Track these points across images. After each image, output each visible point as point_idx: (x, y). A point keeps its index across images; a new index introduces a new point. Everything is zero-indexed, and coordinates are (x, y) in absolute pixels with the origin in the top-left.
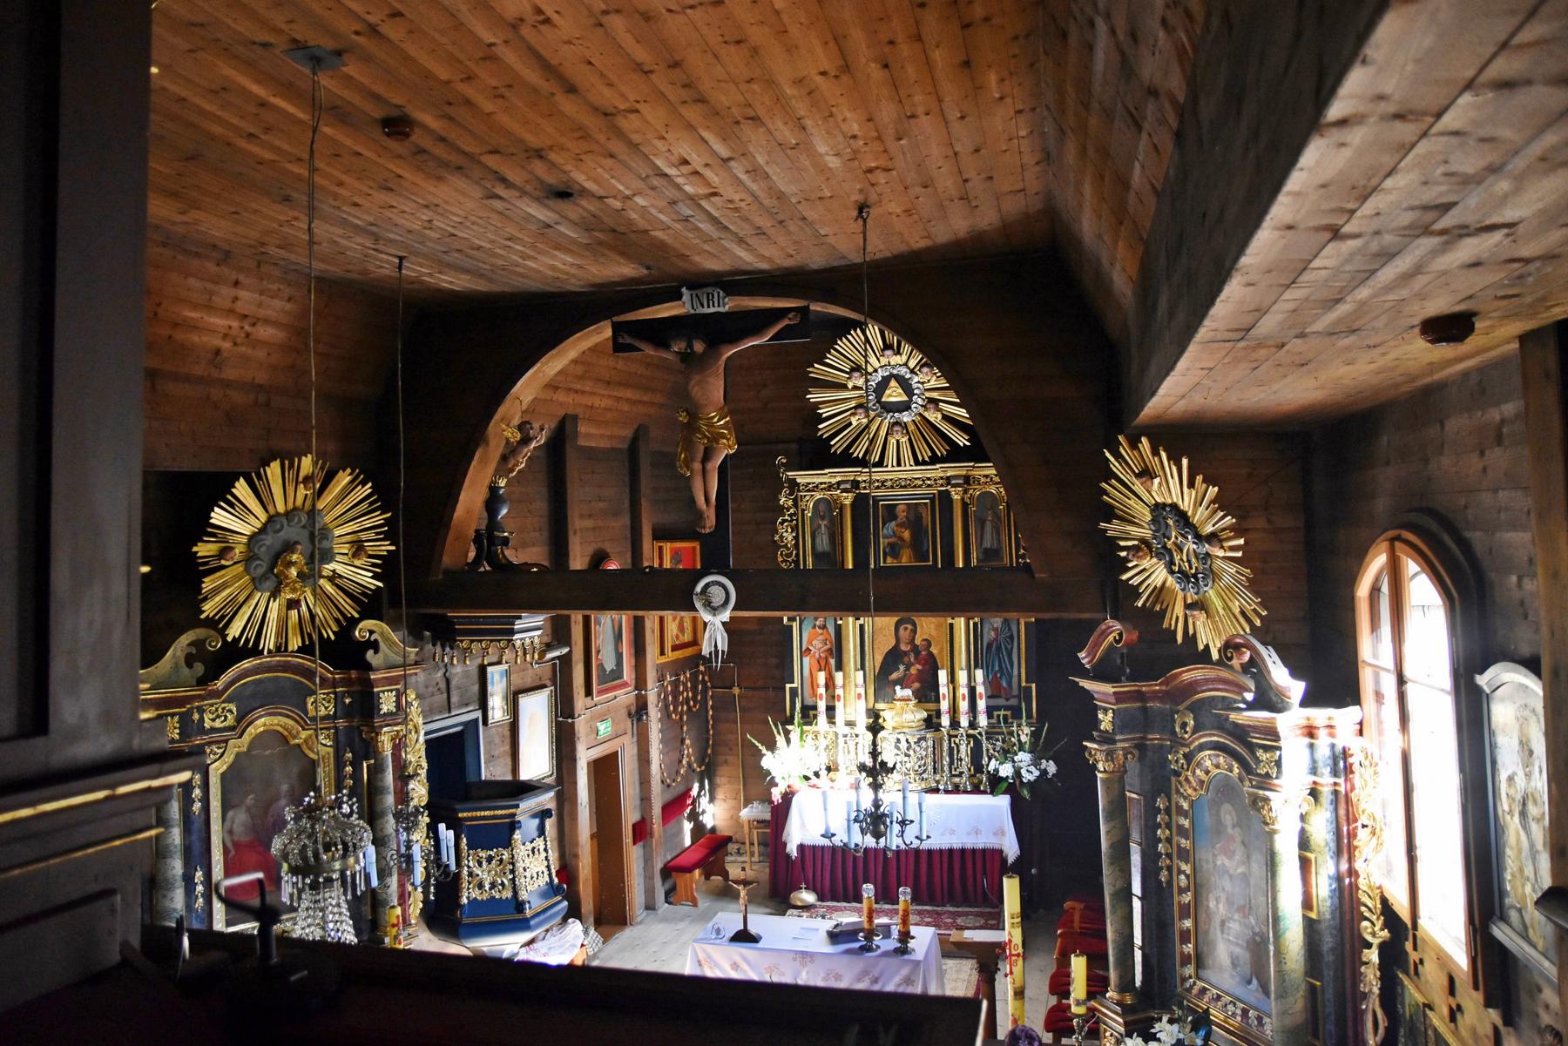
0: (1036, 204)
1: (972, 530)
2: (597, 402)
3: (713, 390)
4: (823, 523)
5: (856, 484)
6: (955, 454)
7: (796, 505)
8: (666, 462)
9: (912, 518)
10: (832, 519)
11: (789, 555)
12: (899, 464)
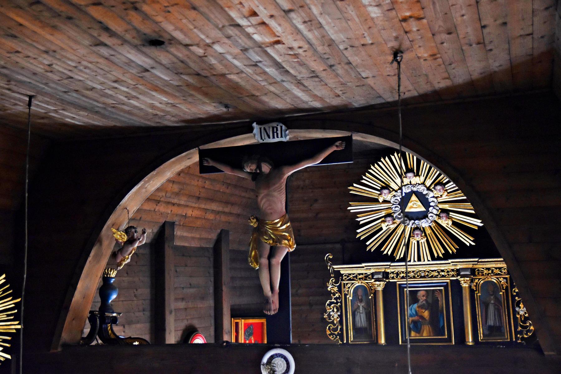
0: (541, 47)
1: (478, 311)
2: (189, 212)
3: (277, 201)
4: (361, 305)
5: (386, 275)
6: (463, 252)
7: (340, 291)
8: (241, 257)
9: (430, 300)
10: (368, 302)
11: (336, 330)
12: (419, 260)
